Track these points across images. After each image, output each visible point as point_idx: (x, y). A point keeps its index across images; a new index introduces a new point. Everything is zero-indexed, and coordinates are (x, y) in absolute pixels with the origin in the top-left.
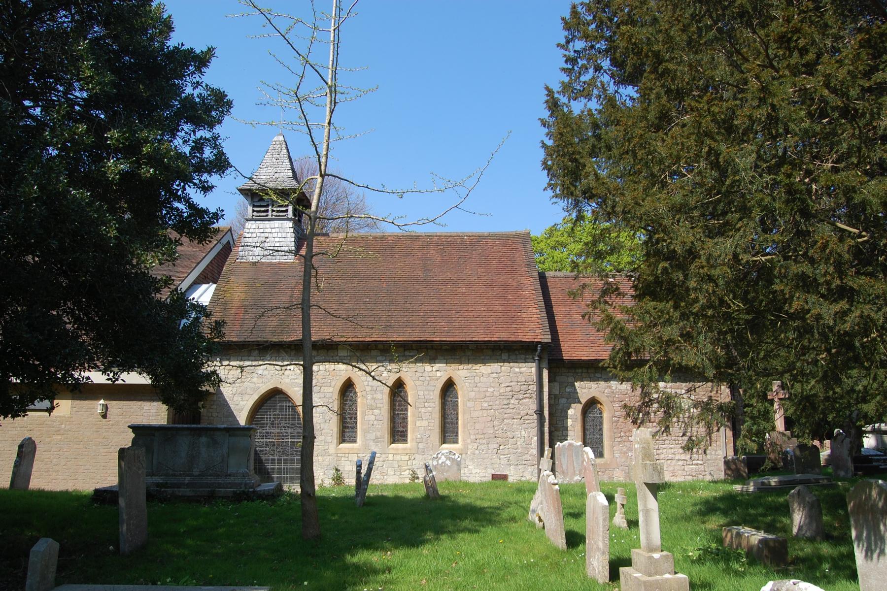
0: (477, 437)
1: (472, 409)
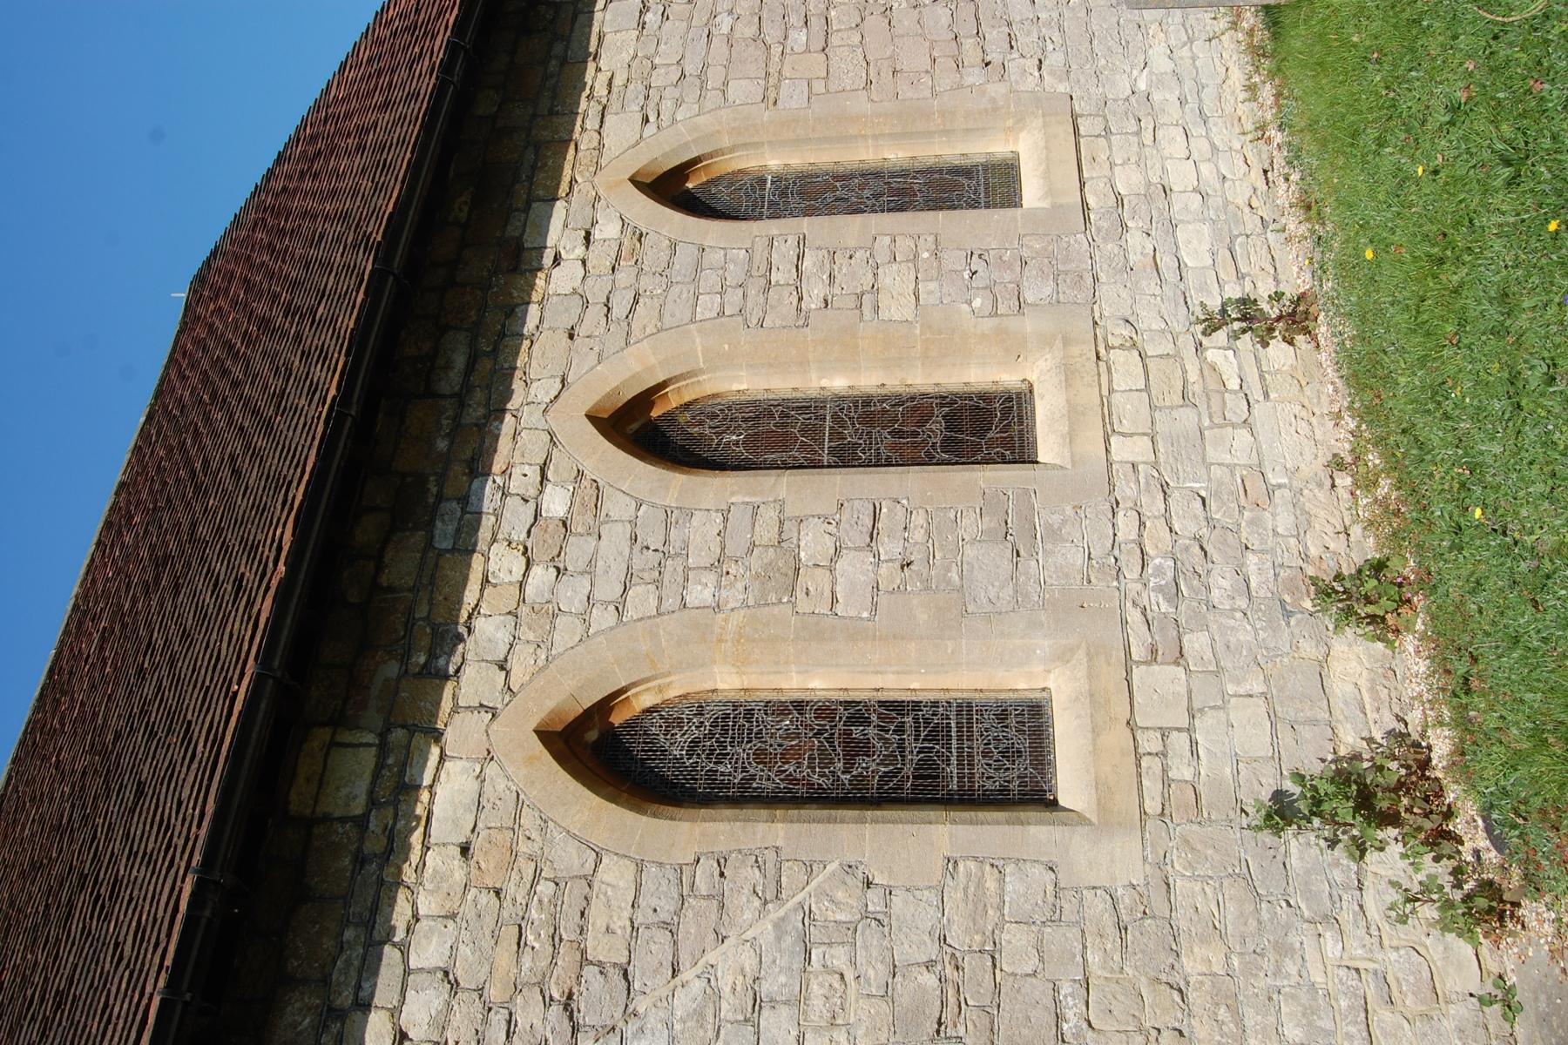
1: (819, 87)
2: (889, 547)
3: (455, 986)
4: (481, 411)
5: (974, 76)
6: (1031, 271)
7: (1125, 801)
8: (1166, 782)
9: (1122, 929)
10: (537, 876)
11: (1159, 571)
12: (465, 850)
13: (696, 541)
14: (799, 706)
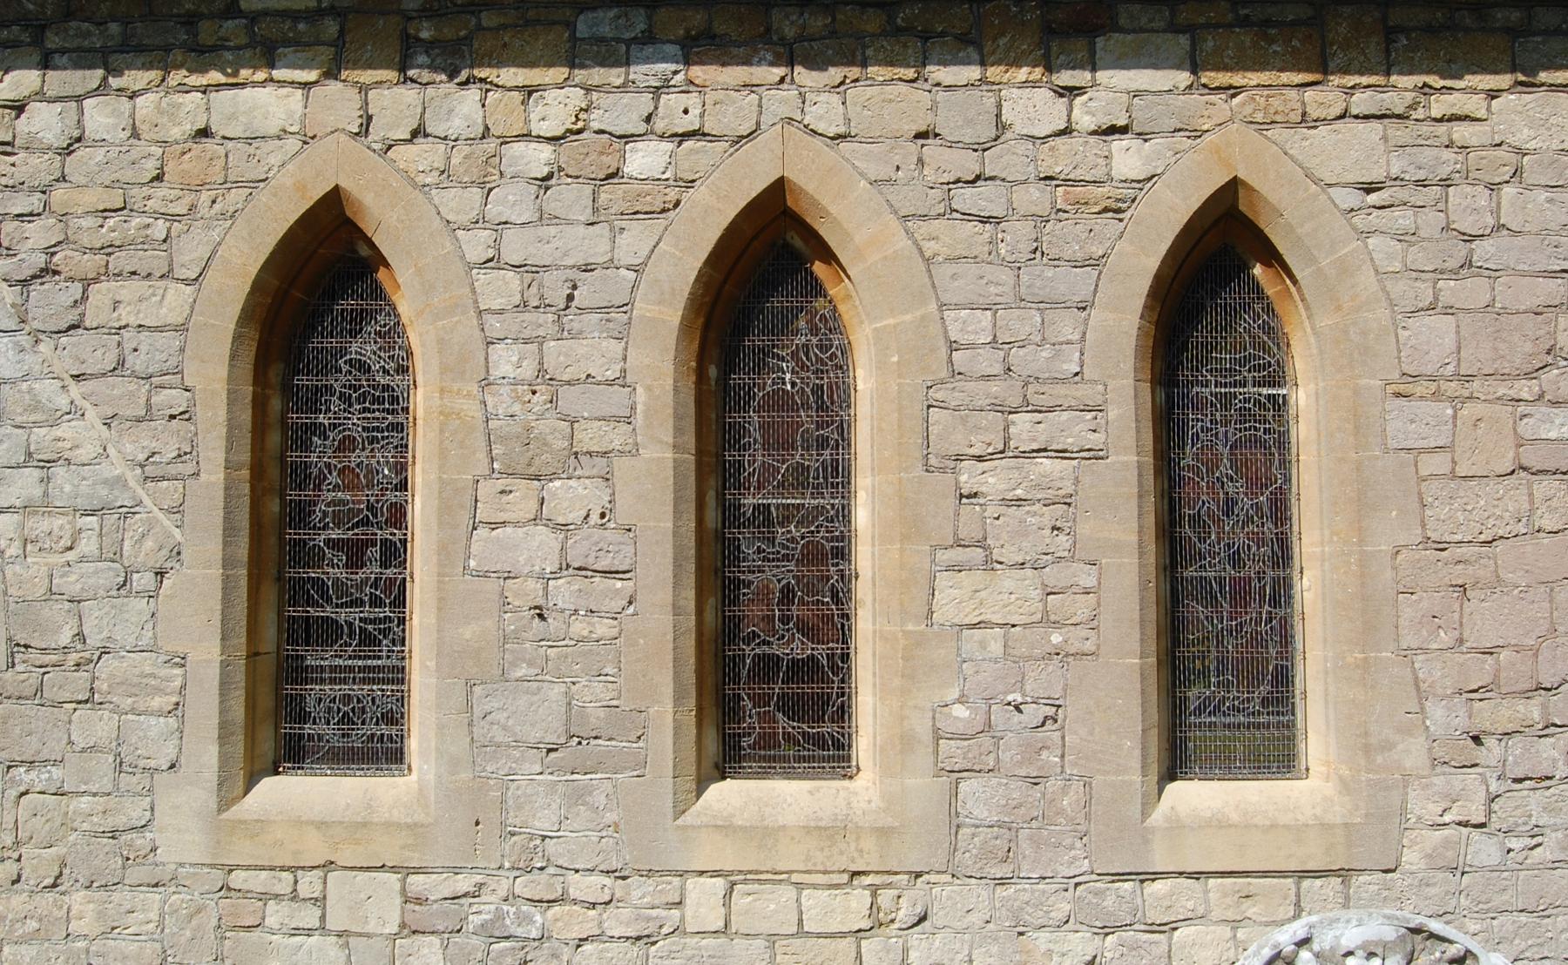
0: (1494, 714)
1: (1435, 464)
2: (564, 592)
3: (68, 151)
4: (790, 32)
5: (1444, 717)
6: (1017, 790)
7: (241, 852)
8: (265, 897)
9: (114, 834)
10: (173, 218)
11: (526, 919)
12: (204, 133)
13: (580, 347)
14: (403, 486)
